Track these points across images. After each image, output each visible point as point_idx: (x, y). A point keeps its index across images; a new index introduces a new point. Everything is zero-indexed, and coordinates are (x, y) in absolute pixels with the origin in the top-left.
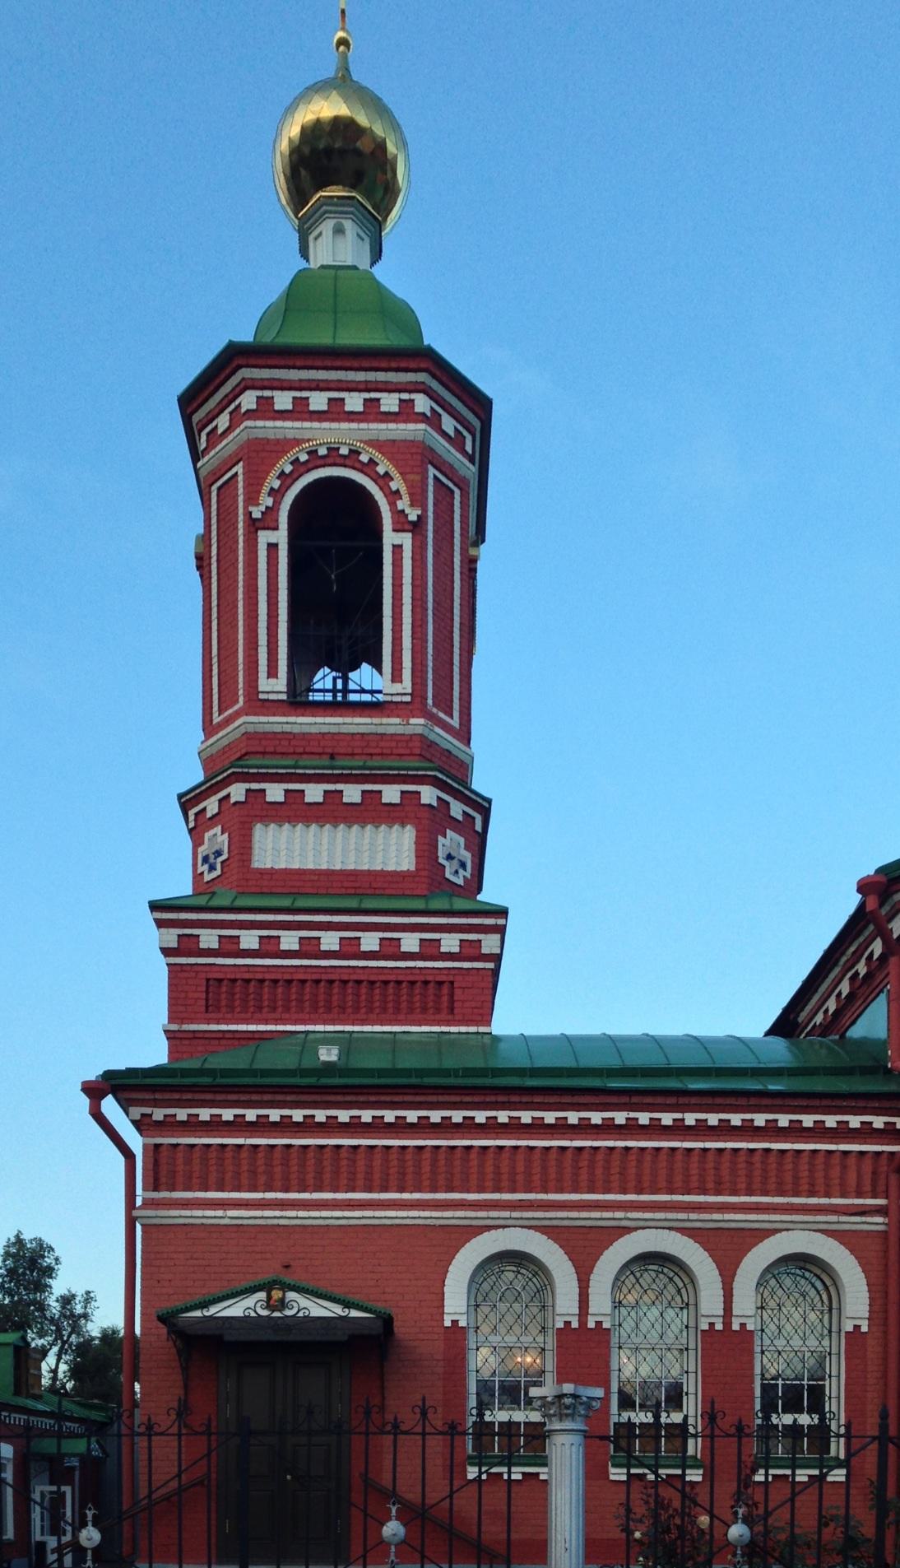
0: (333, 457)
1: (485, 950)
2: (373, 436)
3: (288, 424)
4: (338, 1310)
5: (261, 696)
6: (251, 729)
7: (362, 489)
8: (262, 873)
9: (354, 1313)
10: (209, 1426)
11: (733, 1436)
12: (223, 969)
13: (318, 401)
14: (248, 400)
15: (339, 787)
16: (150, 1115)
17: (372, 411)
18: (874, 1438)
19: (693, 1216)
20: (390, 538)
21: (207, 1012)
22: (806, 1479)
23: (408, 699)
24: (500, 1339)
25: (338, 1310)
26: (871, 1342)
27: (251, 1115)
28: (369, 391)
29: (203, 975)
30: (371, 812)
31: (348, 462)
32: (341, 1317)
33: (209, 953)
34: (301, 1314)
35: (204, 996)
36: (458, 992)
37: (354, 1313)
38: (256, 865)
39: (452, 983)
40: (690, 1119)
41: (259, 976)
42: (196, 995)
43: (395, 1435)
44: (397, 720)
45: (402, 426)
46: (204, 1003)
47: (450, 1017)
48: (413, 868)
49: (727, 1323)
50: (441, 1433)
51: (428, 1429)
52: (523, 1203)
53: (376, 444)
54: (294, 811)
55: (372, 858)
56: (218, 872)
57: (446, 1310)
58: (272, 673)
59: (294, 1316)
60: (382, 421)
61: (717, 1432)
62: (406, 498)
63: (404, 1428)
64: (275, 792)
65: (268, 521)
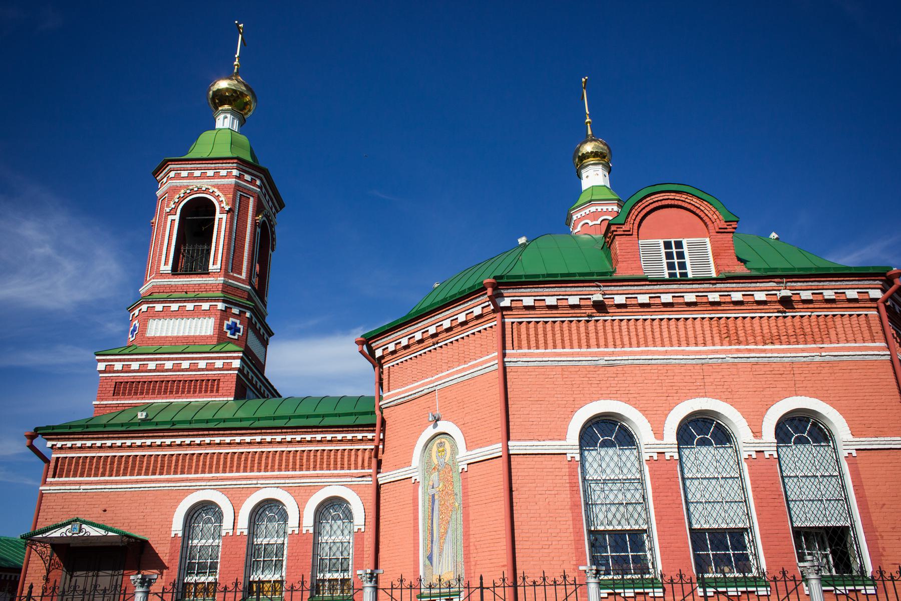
0: (199, 190)
1: (233, 366)
2: (213, 184)
3: (185, 181)
4: (102, 532)
5: (161, 272)
6: (154, 284)
7: (210, 200)
8: (149, 338)
9: (110, 534)
10: (575, 581)
11: (552, 585)
12: (123, 378)
13: (197, 173)
14: (172, 174)
15: (185, 304)
16: (56, 445)
17: (216, 176)
18: (26, 597)
19: (287, 481)
20: (218, 215)
21: (114, 395)
22: (606, 595)
23: (219, 271)
24: (604, 527)
25: (102, 532)
26: (366, 536)
27: (89, 443)
28: (215, 169)
29: (114, 381)
30: (197, 313)
31: (198, 192)
32: (104, 536)
33: (118, 372)
34: (86, 535)
35: (113, 389)
36: (221, 383)
37: (110, 534)
38: (148, 335)
39: (219, 380)
40: (289, 438)
41: (138, 380)
42: (110, 389)
43: (534, 586)
44: (212, 279)
45: (227, 180)
46: (113, 392)
47: (217, 394)
48: (212, 334)
49: (300, 531)
50: (510, 586)
51: (526, 584)
52: (213, 478)
53: (214, 186)
54: (166, 314)
55: (195, 330)
56: (225, 330)
57: (173, 529)
58: (166, 263)
59: (83, 536)
60: (220, 178)
61: (304, 588)
62: (225, 203)
63: (433, 586)
64: (159, 307)
65: (172, 212)
